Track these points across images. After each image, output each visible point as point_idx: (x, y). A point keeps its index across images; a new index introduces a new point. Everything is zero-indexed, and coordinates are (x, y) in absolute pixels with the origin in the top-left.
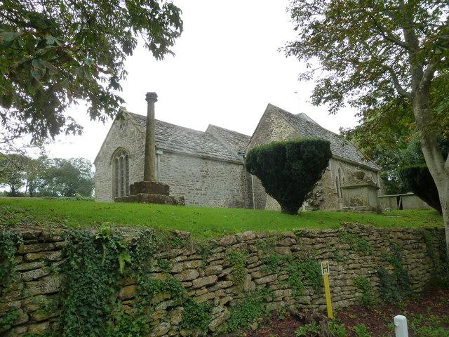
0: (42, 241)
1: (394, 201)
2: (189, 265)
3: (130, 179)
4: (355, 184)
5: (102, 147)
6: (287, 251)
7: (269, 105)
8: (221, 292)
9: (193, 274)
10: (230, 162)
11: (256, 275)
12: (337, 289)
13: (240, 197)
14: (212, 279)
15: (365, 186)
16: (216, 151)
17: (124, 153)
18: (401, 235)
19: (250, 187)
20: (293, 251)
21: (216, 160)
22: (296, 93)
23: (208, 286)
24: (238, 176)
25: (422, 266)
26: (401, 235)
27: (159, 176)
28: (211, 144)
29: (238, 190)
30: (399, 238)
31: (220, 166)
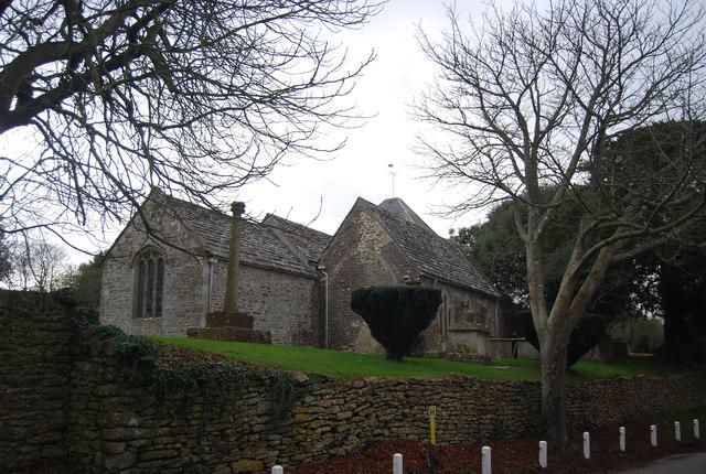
0: (258, 380)
1: (509, 346)
2: (334, 402)
3: (165, 292)
4: (463, 327)
5: (116, 241)
6: (401, 396)
7: (359, 198)
8: (354, 425)
9: (337, 409)
10: (297, 276)
11: (379, 413)
12: (440, 432)
13: (308, 326)
14: (350, 414)
15: (476, 331)
16: (281, 258)
17: (156, 253)
18: (500, 387)
19: (322, 311)
20: (407, 396)
21: (280, 272)
22: (390, 166)
23: (347, 419)
24: (308, 295)
25: (518, 418)
26: (500, 387)
27: (242, 306)
28: (273, 246)
29: (306, 316)
30: (498, 390)
31: (286, 281)
